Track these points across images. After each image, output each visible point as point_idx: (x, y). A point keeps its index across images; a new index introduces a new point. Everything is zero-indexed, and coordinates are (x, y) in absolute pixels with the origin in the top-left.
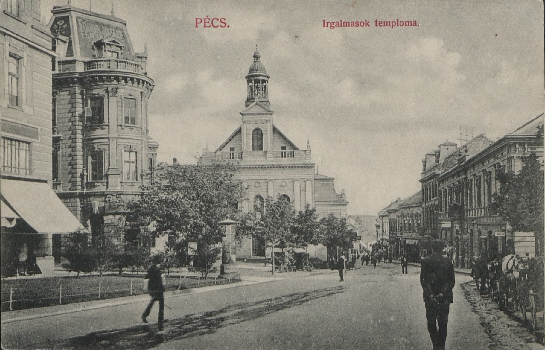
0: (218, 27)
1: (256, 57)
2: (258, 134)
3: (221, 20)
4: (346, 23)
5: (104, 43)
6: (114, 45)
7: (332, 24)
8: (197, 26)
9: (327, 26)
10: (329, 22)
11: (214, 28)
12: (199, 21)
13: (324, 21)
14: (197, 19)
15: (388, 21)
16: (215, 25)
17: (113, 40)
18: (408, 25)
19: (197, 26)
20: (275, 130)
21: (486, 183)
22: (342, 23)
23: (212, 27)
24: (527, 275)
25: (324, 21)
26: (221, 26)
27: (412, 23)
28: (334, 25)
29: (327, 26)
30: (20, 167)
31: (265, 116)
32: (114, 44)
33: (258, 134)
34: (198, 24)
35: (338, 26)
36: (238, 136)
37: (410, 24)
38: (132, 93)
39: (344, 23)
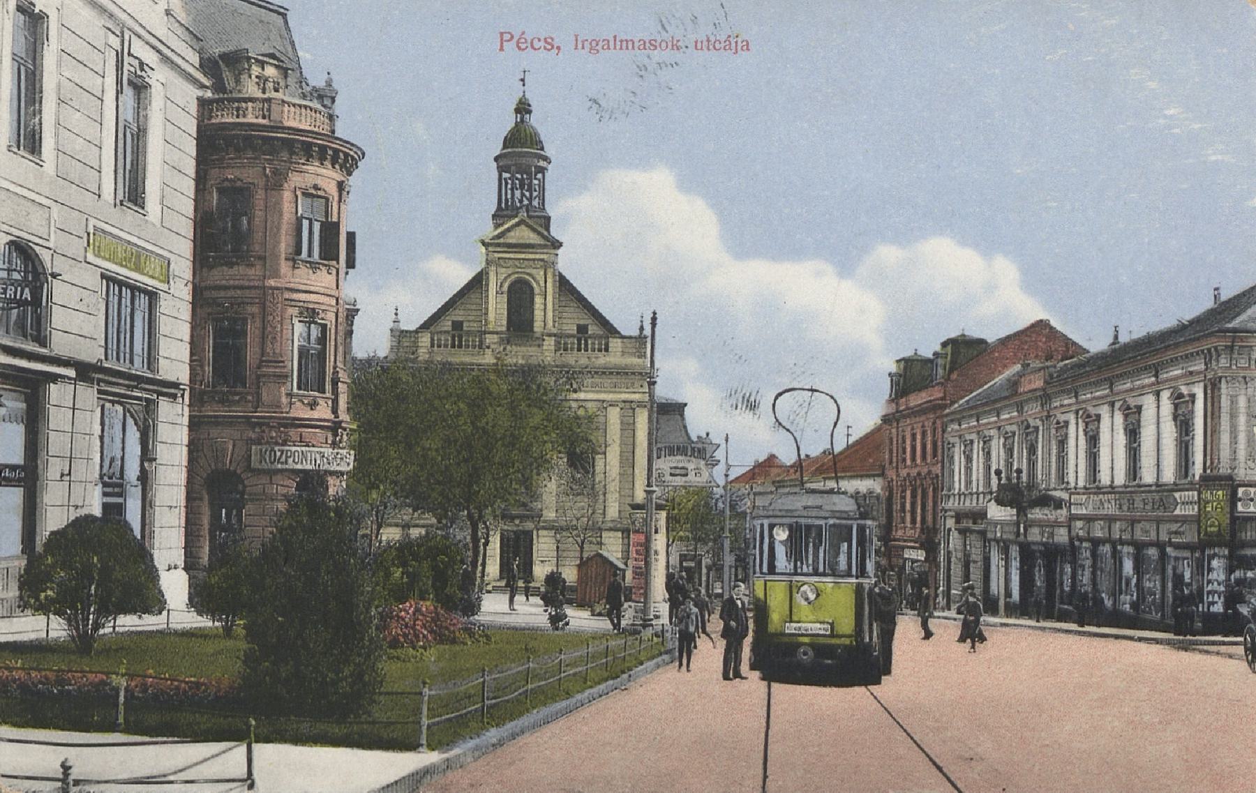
0: (539, 49)
1: (523, 108)
2: (520, 296)
3: (545, 39)
4: (627, 41)
5: (249, 58)
6: (271, 64)
7: (594, 44)
8: (502, 49)
9: (583, 48)
10: (587, 40)
11: (533, 51)
12: (507, 37)
13: (576, 36)
14: (502, 34)
15: (629, 38)
16: (536, 47)
17: (271, 51)
18: (627, 48)
19: (502, 49)
20: (564, 286)
21: (962, 456)
22: (580, 40)
23: (529, 48)
24: (224, 510)
25: (576, 36)
26: (545, 48)
27: (637, 44)
28: (599, 48)
29: (583, 48)
30: (70, 434)
31: (140, 161)
32: (271, 61)
33: (520, 296)
34: (505, 44)
35: (609, 48)
36: (474, 296)
37: (630, 47)
38: (320, 182)
39: (621, 41)
